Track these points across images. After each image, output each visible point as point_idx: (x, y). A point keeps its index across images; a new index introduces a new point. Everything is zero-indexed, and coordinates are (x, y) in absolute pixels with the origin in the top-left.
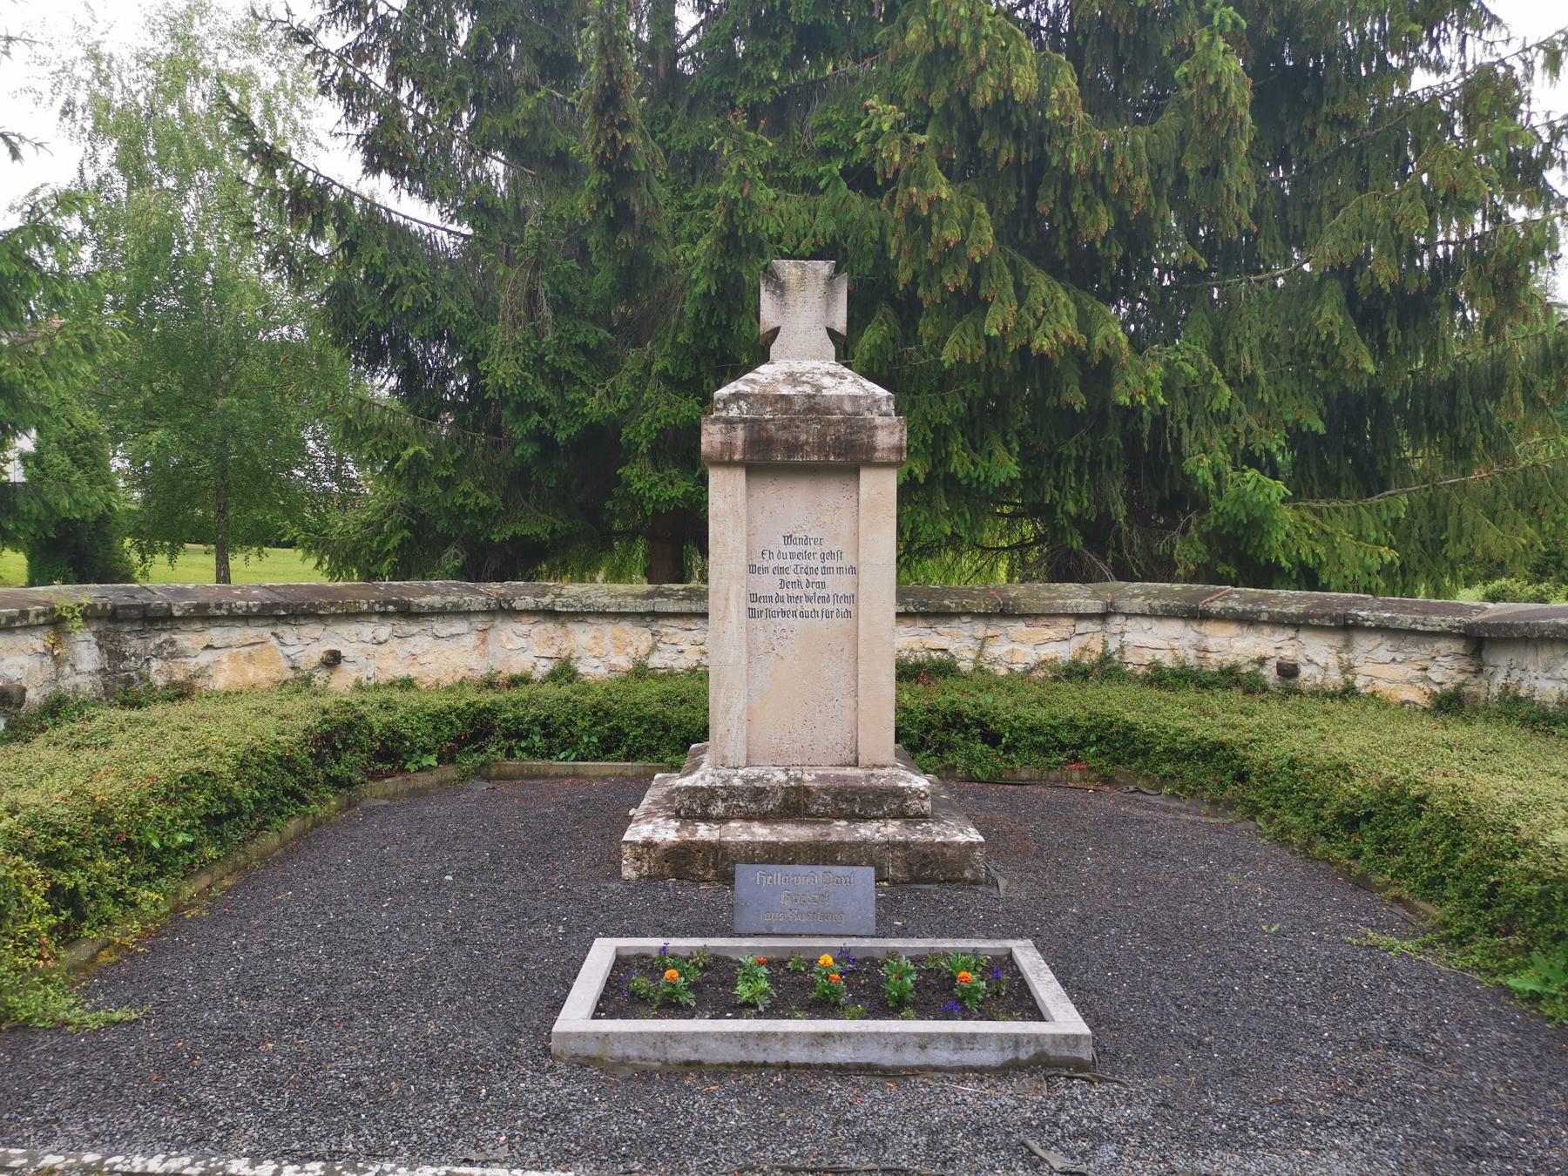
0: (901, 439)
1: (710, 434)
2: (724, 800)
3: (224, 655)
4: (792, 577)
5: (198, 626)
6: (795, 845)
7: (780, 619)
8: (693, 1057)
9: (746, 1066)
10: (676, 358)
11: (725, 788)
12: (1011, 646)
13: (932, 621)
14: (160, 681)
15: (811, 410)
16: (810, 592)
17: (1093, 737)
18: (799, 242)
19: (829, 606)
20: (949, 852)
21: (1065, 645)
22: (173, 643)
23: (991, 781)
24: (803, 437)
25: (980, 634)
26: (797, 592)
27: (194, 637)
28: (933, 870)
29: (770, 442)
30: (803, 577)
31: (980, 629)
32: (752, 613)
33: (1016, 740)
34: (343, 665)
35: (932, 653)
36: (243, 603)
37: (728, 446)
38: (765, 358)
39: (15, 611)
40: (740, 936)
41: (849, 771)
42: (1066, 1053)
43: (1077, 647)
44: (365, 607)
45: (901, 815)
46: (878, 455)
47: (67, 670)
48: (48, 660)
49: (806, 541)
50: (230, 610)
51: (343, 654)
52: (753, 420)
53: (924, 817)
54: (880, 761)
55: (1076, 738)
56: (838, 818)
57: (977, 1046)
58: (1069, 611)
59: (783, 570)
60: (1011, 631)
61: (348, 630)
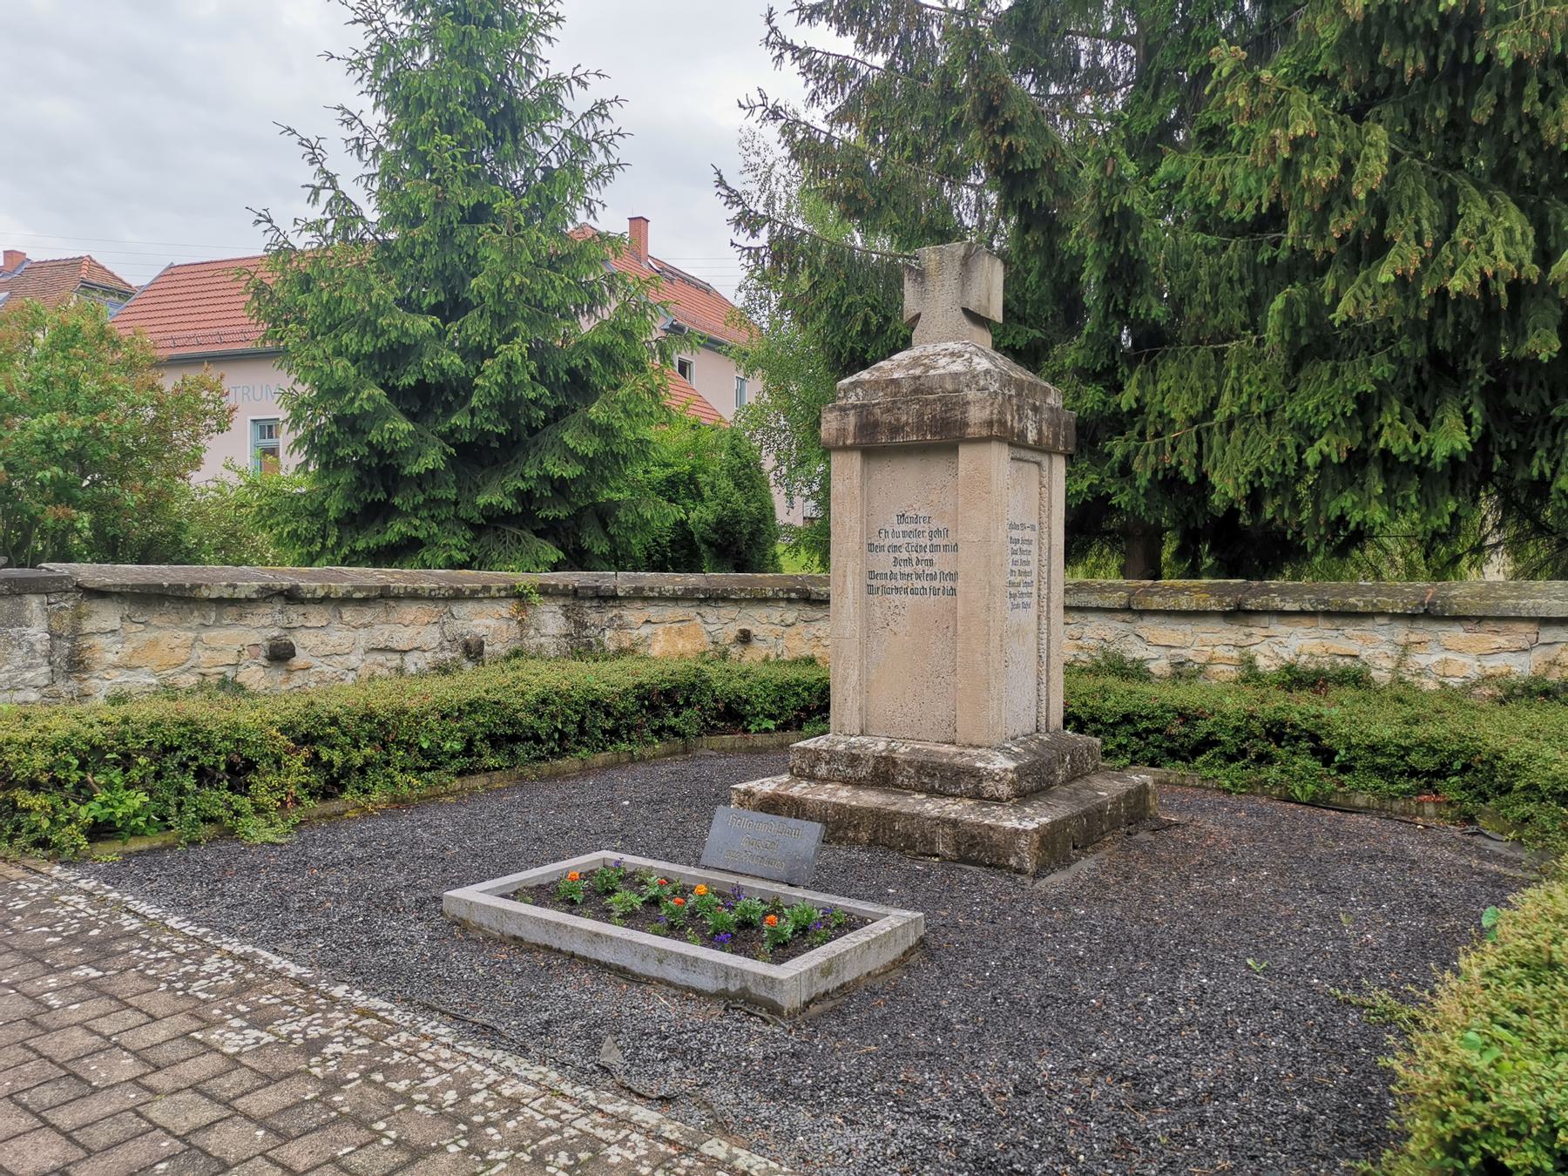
0: (992, 413)
1: (828, 422)
2: (827, 763)
3: (660, 629)
4: (904, 555)
5: (639, 604)
6: (859, 809)
7: (893, 596)
8: (518, 934)
9: (548, 948)
10: (1091, 349)
11: (827, 751)
12: (1443, 656)
13: (1338, 622)
14: (612, 647)
15: (916, 391)
16: (920, 568)
17: (1457, 765)
18: (1243, 206)
19: (936, 584)
20: (995, 837)
21: (1524, 658)
22: (621, 617)
23: (1313, 803)
24: (904, 418)
25: (1401, 639)
26: (908, 570)
27: (636, 613)
28: (980, 852)
29: (876, 424)
30: (914, 555)
31: (1401, 632)
32: (871, 590)
33: (1354, 759)
34: (756, 644)
35: (1339, 660)
36: (671, 587)
37: (842, 431)
38: (907, 343)
39: (478, 586)
40: (706, 868)
41: (945, 748)
42: (764, 994)
43: (1540, 660)
44: (771, 594)
45: (977, 796)
46: (970, 430)
47: (532, 632)
48: (514, 624)
49: (916, 519)
50: (660, 592)
51: (754, 631)
52: (863, 406)
53: (998, 801)
54: (976, 742)
55: (1430, 764)
56: (920, 792)
57: (698, 970)
58: (1524, 614)
59: (896, 548)
60: (1443, 637)
61: (759, 613)
